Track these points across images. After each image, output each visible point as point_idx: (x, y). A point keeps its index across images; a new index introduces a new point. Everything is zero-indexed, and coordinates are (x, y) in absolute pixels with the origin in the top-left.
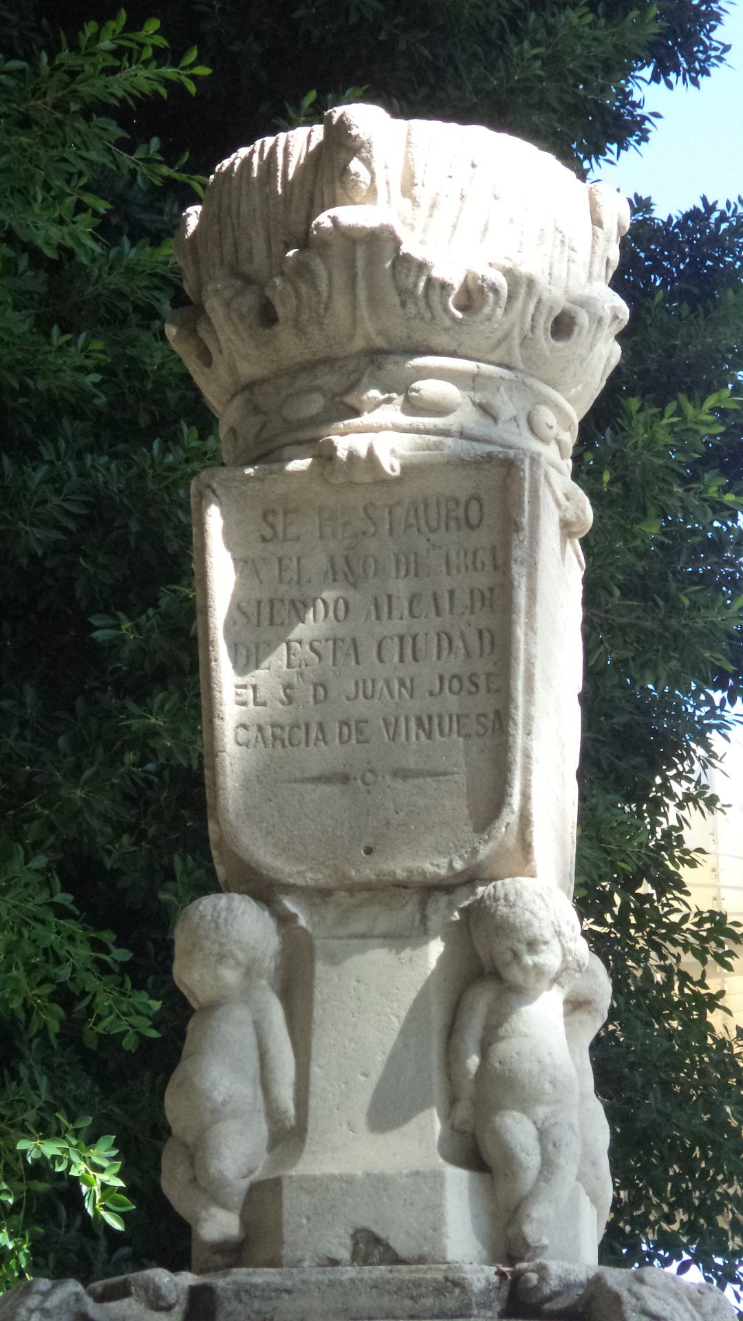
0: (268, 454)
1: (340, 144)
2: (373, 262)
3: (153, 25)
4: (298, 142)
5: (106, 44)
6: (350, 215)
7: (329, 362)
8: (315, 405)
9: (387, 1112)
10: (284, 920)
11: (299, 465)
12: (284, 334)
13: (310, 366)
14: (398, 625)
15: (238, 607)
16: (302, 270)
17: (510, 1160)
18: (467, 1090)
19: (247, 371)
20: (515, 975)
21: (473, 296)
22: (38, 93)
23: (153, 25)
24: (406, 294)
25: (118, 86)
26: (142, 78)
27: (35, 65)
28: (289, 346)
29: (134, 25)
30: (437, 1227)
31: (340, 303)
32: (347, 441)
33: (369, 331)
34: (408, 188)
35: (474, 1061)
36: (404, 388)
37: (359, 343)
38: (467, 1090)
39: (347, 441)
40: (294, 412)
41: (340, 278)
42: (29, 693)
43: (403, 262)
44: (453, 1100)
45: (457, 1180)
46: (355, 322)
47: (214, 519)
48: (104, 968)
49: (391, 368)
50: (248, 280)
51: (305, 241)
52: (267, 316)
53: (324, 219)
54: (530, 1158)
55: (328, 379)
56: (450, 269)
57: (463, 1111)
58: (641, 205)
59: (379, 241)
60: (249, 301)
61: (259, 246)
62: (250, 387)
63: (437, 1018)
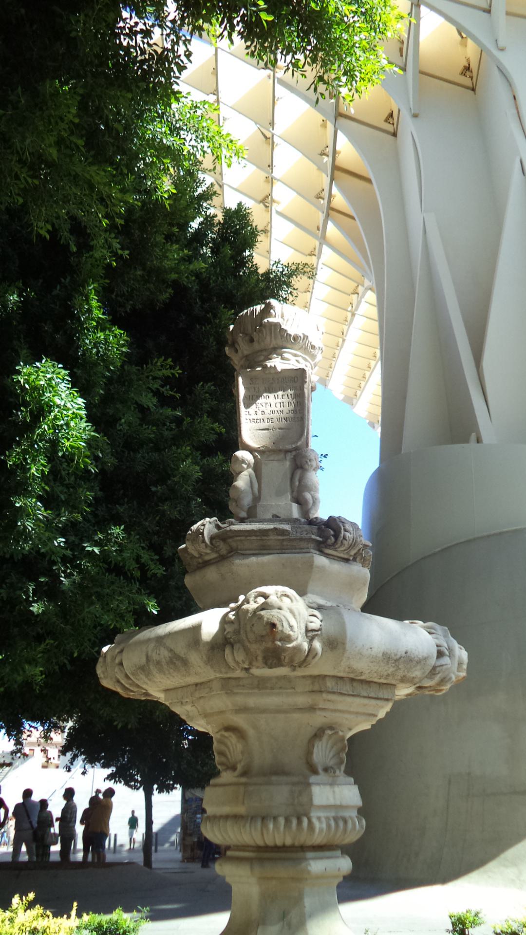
0: (253, 366)
1: (269, 307)
2: (275, 329)
3: (170, 360)
4: (259, 308)
5: (159, 364)
6: (271, 320)
7: (265, 350)
8: (262, 358)
9: (279, 494)
10: (255, 457)
11: (259, 369)
12: (255, 344)
13: (261, 351)
14: (279, 401)
15: (245, 396)
16: (260, 331)
17: (306, 502)
18: (296, 489)
19: (246, 353)
20: (307, 467)
21: (296, 338)
22: (143, 374)
23: (170, 360)
24: (282, 336)
25: (160, 374)
26: (167, 372)
27: (143, 368)
28: (256, 346)
29: (165, 360)
30: (292, 512)
31: (268, 338)
32: (269, 364)
33: (274, 343)
34: (282, 316)
35: (297, 483)
36: (281, 355)
37: (272, 346)
38: (296, 489)
39: (269, 364)
40: (255, 360)
41: (268, 333)
42: (135, 503)
43: (282, 330)
44: (292, 492)
45: (295, 506)
46: (270, 341)
47: (240, 380)
48: (152, 560)
49: (279, 351)
50: (247, 335)
51: (261, 325)
52: (252, 340)
53: (266, 320)
54: (311, 502)
55: (265, 353)
56: (292, 331)
57: (295, 494)
58: (28, 793)
59: (277, 326)
60: (247, 338)
61: (250, 328)
62: (247, 356)
63: (289, 476)
